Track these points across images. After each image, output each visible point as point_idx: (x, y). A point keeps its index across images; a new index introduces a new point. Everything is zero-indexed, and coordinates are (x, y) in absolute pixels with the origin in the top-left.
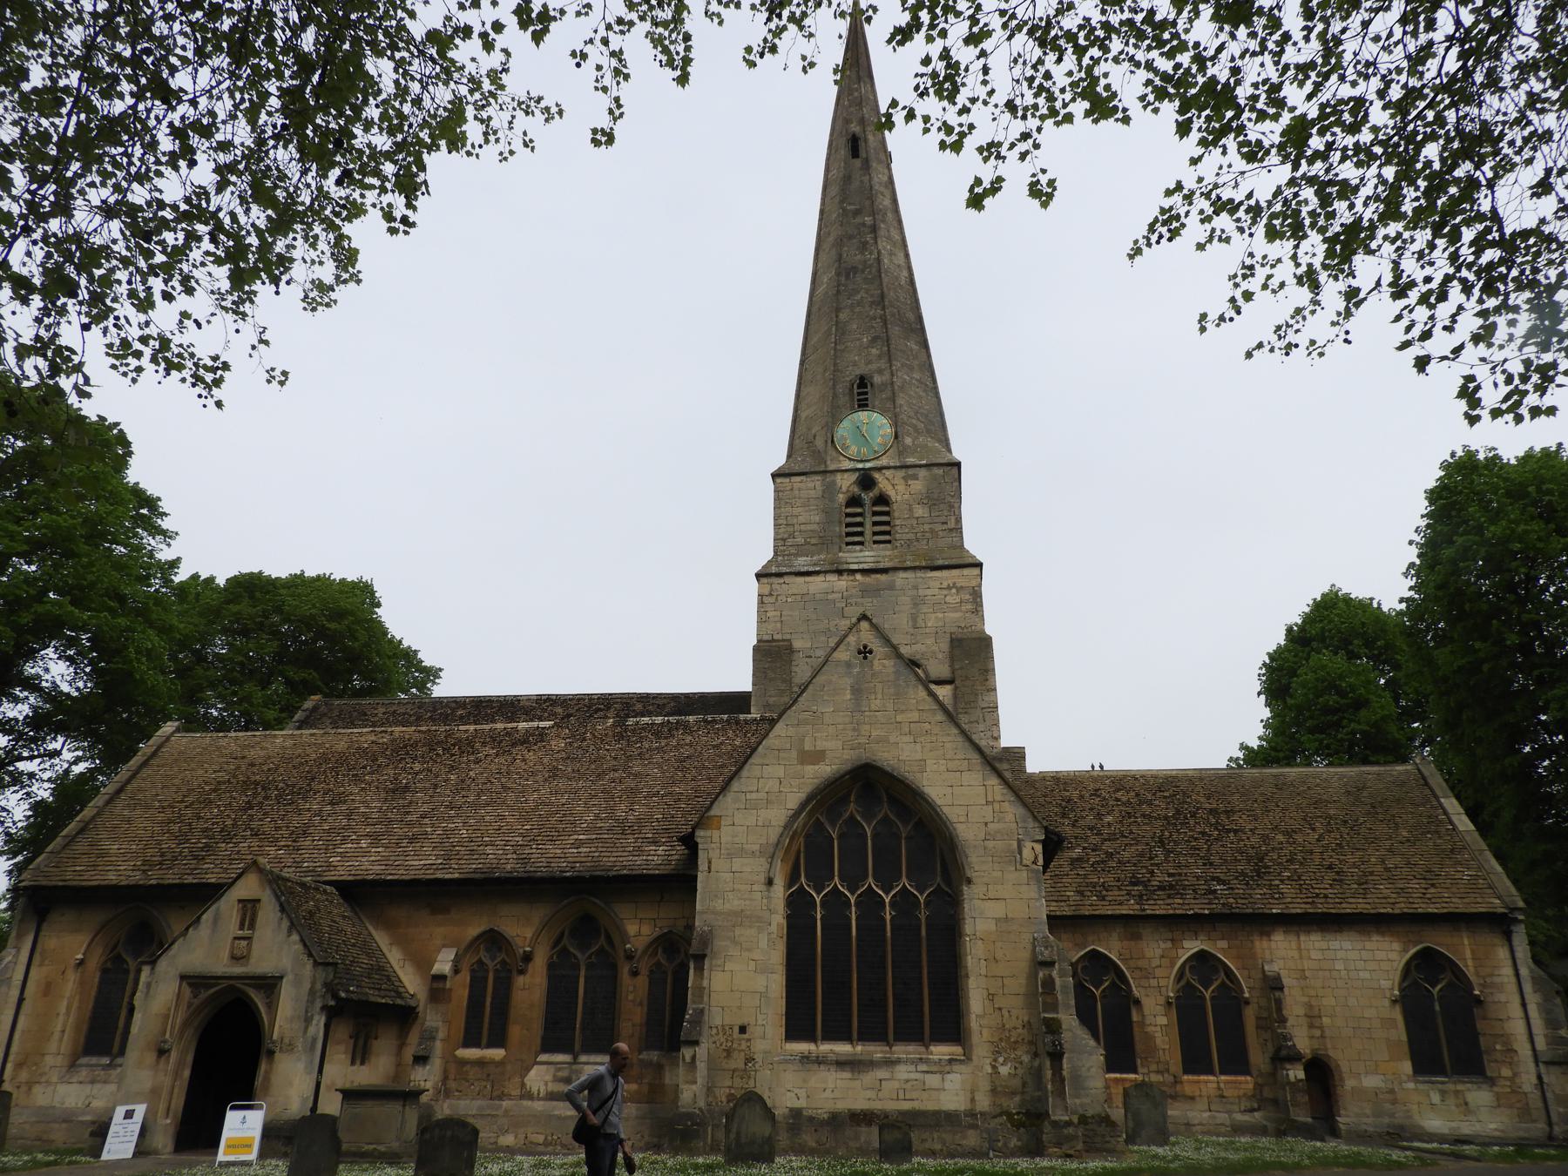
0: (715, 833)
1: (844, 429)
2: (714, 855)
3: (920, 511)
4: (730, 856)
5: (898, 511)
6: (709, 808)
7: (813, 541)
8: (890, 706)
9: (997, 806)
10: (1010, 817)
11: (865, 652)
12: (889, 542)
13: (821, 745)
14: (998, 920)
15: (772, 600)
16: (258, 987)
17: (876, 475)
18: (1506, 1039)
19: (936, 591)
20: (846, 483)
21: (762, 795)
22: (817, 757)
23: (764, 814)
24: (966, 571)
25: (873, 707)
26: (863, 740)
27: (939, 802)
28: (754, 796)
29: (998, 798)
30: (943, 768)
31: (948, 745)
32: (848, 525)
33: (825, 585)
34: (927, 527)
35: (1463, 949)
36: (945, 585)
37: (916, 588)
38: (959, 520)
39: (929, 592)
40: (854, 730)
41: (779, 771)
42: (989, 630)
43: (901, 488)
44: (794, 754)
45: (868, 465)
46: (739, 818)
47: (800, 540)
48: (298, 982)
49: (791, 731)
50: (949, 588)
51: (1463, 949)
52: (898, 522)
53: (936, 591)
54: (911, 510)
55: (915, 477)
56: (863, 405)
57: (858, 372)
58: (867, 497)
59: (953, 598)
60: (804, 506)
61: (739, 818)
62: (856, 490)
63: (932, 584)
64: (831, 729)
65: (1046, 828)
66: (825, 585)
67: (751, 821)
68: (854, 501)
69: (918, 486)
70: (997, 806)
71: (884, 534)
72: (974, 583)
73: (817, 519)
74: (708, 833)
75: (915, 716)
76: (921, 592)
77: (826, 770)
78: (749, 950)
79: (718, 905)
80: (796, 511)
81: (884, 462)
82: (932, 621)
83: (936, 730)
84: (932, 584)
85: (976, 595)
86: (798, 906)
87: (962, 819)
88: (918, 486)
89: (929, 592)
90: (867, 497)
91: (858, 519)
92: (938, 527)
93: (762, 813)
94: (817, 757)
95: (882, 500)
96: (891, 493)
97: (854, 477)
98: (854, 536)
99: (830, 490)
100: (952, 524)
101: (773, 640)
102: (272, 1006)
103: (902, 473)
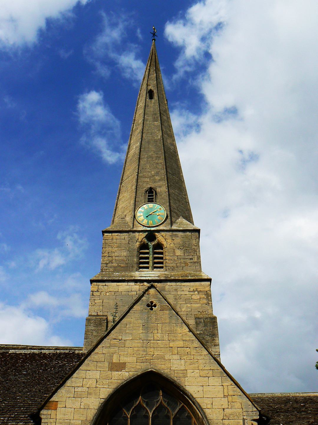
0: (52, 412)
1: (141, 213)
3: (179, 253)
5: (167, 256)
6: (51, 397)
7: (122, 265)
8: (166, 338)
9: (230, 398)
10: (238, 405)
12: (162, 267)
13: (123, 359)
15: (98, 294)
19: (187, 293)
20: (141, 237)
21: (85, 389)
22: (121, 366)
23: (85, 401)
24: (203, 283)
25: (156, 338)
27: (195, 396)
28: (80, 389)
29: (231, 393)
30: (198, 375)
31: (200, 361)
33: (128, 287)
34: (182, 261)
36: (192, 289)
37: (176, 290)
38: (199, 257)
39: (182, 293)
40: (144, 351)
42: (215, 314)
43: (169, 241)
44: (106, 364)
45: (153, 229)
46: (69, 403)
47: (115, 264)
49: (105, 351)
50: (194, 291)
52: (167, 254)
53: (187, 293)
54: (174, 252)
55: (177, 236)
56: (150, 201)
57: (149, 186)
58: (151, 244)
59: (196, 297)
60: (118, 247)
62: (146, 241)
63: (185, 289)
64: (130, 350)
65: (260, 411)
66: (128, 287)
67: (77, 405)
68: (144, 246)
69: (178, 240)
70: (230, 398)
71: (158, 264)
72: (207, 289)
73: (125, 254)
74: (49, 412)
75: (181, 344)
76: (179, 293)
77: (125, 375)
80: (114, 250)
81: (161, 228)
83: (193, 352)
84: (185, 289)
85: (208, 295)
87: (209, 406)
88: (178, 240)
89: (182, 293)
90: (151, 244)
91: (141, 255)
92: (188, 261)
94: (121, 366)
95: (159, 246)
96: (164, 243)
97: (145, 234)
98: (142, 265)
100: (195, 260)
101: (98, 315)
103: (170, 233)
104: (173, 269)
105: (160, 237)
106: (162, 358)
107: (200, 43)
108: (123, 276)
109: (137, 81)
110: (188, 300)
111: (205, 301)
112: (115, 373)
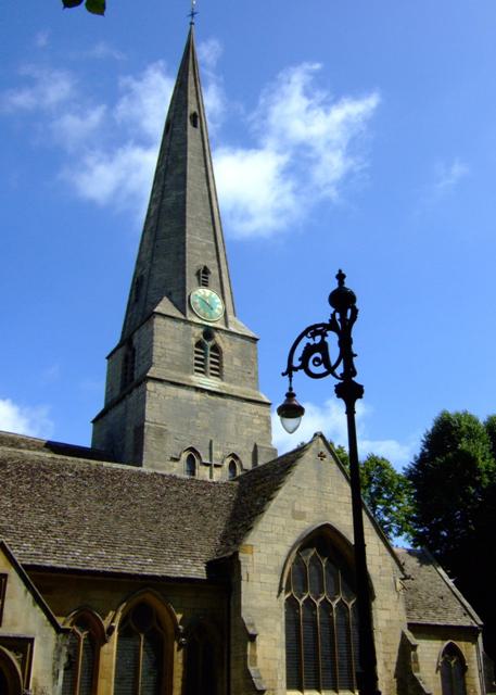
2: (250, 570)
4: (259, 572)
7: (178, 363)
11: (321, 456)
13: (304, 509)
14: (387, 621)
16: (15, 650)
17: (216, 334)
18: (473, 686)
26: (323, 509)
32: (196, 359)
35: (462, 645)
41: (283, 521)
43: (228, 345)
44: (290, 512)
45: (211, 324)
46: (262, 547)
47: (168, 360)
48: (45, 641)
50: (255, 414)
51: (462, 645)
54: (232, 360)
59: (257, 421)
60: (172, 337)
61: (262, 547)
64: (308, 500)
68: (199, 344)
71: (218, 372)
78: (271, 632)
79: (253, 602)
82: (246, 432)
86: (291, 604)
91: (202, 357)
93: (275, 546)
95: (216, 348)
96: (222, 345)
98: (201, 368)
99: (187, 333)
100: (252, 375)
102: (27, 662)
104: (231, 382)
105: (219, 338)
106: (333, 511)
107: (360, 119)
108: (180, 378)
109: (218, 84)
110: (249, 424)
111: (265, 428)
112: (298, 522)
